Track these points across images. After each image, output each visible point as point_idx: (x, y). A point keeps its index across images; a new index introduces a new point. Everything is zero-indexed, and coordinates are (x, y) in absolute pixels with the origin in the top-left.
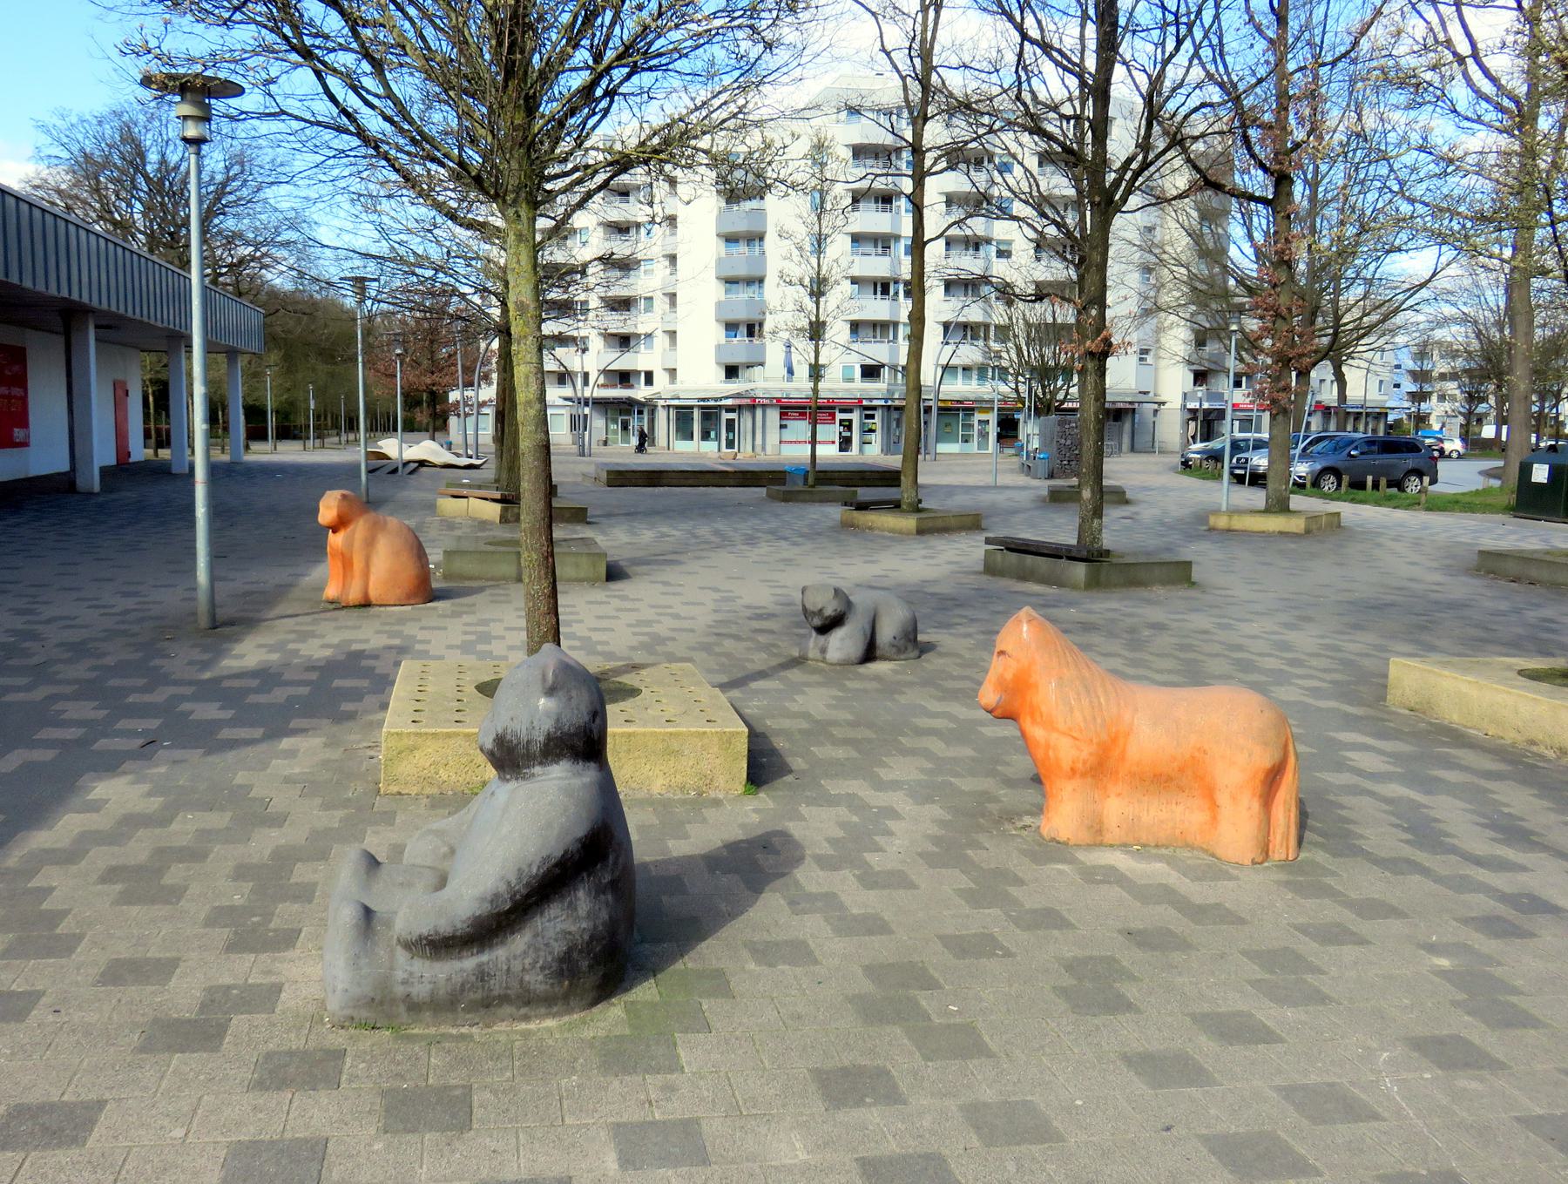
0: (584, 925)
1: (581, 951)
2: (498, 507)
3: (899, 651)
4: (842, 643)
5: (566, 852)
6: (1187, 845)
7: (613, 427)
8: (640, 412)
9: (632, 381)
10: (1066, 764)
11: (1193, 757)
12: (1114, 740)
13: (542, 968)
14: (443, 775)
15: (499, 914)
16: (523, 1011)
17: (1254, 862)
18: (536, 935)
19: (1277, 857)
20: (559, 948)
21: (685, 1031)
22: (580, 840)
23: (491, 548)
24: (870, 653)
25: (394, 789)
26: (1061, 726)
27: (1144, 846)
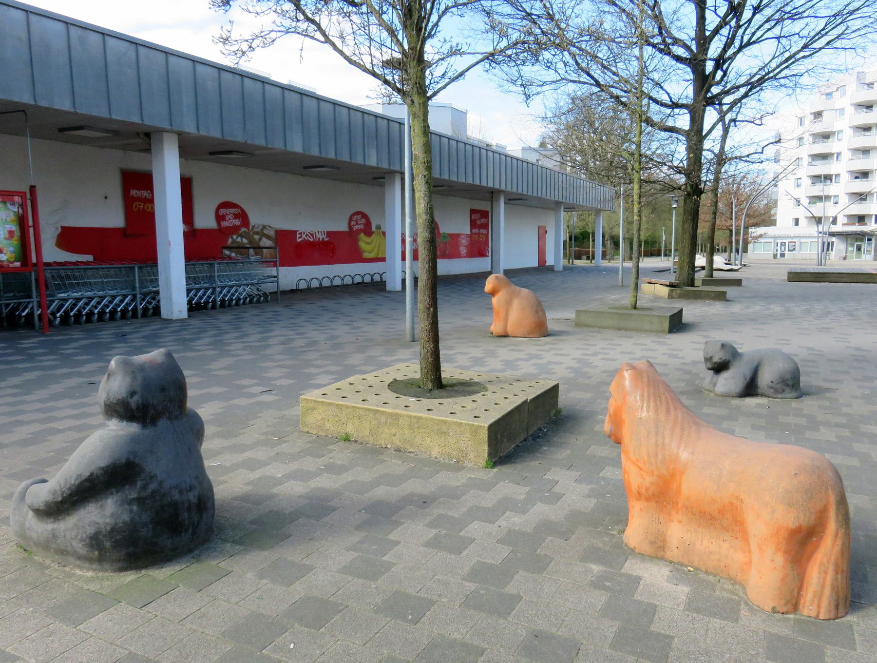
0: (108, 520)
1: (105, 536)
2: (667, 289)
3: (776, 391)
4: (730, 381)
5: (92, 474)
6: (731, 579)
7: (850, 249)
8: (869, 240)
9: (866, 221)
10: (634, 488)
11: (732, 504)
12: (673, 475)
13: (81, 540)
14: (327, 426)
15: (56, 503)
16: (78, 562)
17: (774, 610)
18: (79, 520)
19: (806, 612)
20: (91, 531)
21: (651, 621)
22: (103, 468)
23: (611, 311)
24: (750, 389)
25: (306, 430)
26: (632, 456)
27: (696, 569)
